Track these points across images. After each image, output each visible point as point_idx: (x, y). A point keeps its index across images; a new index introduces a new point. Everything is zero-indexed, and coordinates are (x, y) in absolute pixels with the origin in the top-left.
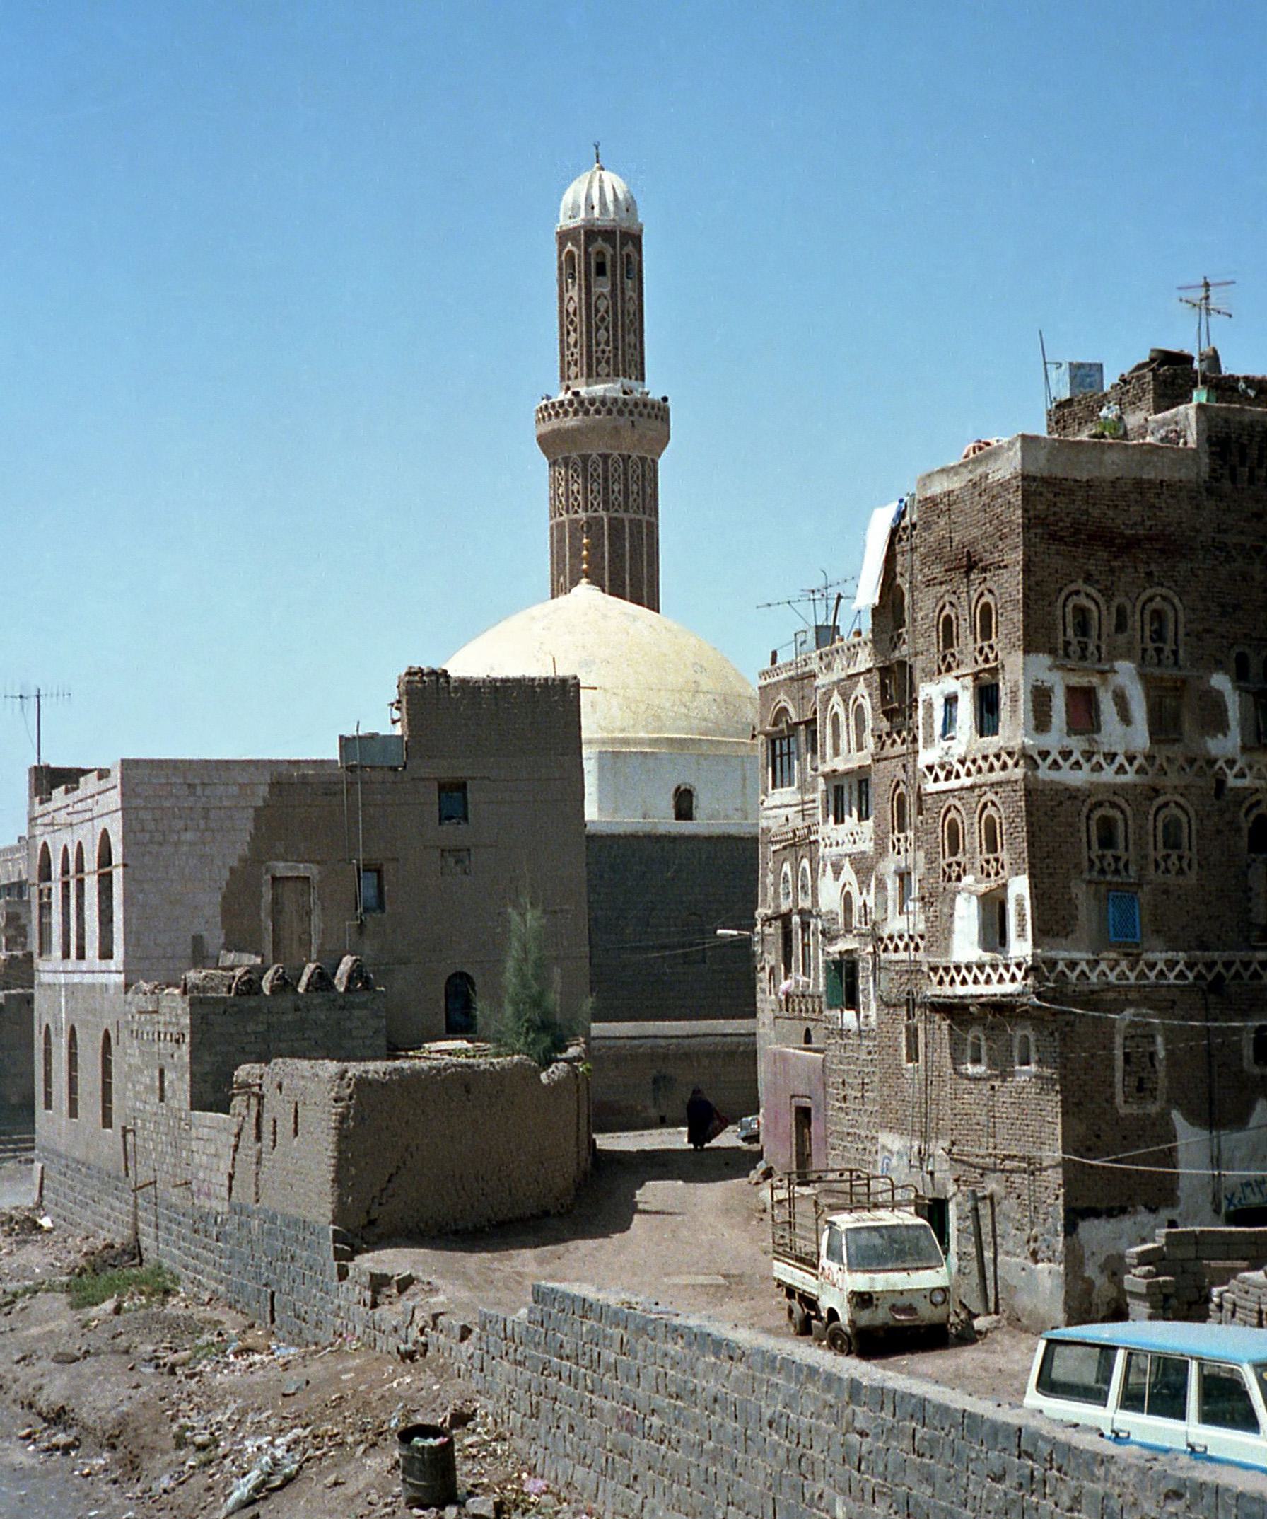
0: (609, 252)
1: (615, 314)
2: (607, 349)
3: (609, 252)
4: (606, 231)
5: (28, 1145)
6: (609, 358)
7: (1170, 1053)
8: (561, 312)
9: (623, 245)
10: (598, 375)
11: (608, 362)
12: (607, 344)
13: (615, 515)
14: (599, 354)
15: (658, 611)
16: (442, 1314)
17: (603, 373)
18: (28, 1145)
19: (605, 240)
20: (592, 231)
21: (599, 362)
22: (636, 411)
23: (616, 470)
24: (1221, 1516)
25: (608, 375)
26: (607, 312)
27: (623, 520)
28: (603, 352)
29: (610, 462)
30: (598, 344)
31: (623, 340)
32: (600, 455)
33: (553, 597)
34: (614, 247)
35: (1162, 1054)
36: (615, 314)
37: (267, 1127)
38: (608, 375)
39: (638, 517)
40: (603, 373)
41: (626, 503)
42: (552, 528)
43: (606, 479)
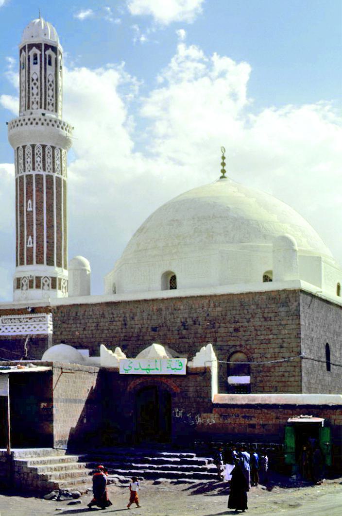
0: (38, 52)
1: (45, 87)
5: (35, 98)
7: (127, 465)
10: (49, 110)
11: (53, 105)
12: (37, 94)
13: (49, 174)
16: (190, 495)
17: (51, 109)
18: (35, 98)
24: (1, 367)
25: (52, 111)
26: (53, 82)
29: (46, 149)
34: (41, 50)
35: (127, 464)
36: (45, 87)
37: (29, 242)
38: (52, 111)
39: (30, 173)
40: (51, 109)
41: (54, 169)
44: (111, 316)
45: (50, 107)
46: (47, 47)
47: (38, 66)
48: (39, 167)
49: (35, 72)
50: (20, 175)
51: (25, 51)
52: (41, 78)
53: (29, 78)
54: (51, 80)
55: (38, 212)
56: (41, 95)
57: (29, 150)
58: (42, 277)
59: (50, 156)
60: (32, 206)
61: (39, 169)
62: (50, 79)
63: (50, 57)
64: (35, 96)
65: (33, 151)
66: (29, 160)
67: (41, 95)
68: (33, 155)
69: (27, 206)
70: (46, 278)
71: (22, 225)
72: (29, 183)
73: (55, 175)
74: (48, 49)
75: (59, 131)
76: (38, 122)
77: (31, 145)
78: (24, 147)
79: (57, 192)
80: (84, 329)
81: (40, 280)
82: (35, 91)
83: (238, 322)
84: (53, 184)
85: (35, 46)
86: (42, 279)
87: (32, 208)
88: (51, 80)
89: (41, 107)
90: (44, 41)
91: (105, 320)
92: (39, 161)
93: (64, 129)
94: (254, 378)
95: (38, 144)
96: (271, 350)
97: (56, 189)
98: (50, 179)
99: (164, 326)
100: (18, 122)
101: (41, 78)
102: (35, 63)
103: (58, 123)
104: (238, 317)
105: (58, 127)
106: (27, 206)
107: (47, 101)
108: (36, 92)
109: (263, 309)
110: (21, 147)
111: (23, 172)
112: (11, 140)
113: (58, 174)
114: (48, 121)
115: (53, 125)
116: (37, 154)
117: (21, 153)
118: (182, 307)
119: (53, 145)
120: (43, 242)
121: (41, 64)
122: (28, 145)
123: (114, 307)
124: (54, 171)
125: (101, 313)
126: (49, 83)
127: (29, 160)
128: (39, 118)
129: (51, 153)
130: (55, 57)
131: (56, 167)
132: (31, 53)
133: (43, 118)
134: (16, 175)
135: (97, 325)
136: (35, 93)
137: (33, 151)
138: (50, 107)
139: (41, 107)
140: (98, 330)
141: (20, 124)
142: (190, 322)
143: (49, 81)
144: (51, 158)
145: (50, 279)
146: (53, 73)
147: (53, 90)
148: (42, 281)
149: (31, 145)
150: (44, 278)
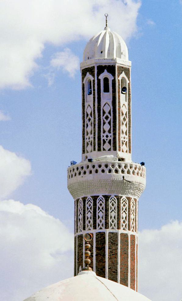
0: (111, 78)
2: (109, 135)
3: (111, 78)
4: (109, 66)
6: (110, 140)
8: (84, 113)
9: (120, 73)
10: (104, 150)
11: (110, 142)
12: (109, 132)
13: (101, 231)
14: (105, 138)
15: (128, 287)
17: (107, 149)
19: (108, 71)
20: (101, 66)
21: (104, 142)
22: (126, 170)
23: (124, 205)
25: (110, 150)
26: (110, 113)
27: (92, 234)
28: (107, 136)
29: (98, 201)
30: (104, 132)
31: (119, 130)
32: (104, 196)
33: (75, 275)
36: (99, 119)
38: (110, 150)
40: (107, 149)
41: (118, 224)
42: (75, 238)
43: (107, 210)
45: (107, 146)
46: (101, 69)
47: (92, 96)
48: (113, 224)
49: (89, 105)
50: (79, 233)
54: (107, 111)
57: (89, 204)
59: (103, 208)
61: (101, 226)
62: (105, 110)
63: (106, 80)
64: (107, 133)
65: (95, 204)
66: (101, 214)
67: (95, 133)
68: (84, 211)
73: (107, 232)
74: (103, 71)
75: (111, 176)
76: (105, 169)
77: (92, 197)
78: (95, 198)
79: (110, 252)
82: (107, 127)
84: (104, 243)
85: (88, 71)
88: (107, 111)
89: (94, 149)
90: (96, 63)
92: (101, 216)
93: (136, 174)
95: (89, 196)
98: (114, 236)
100: (80, 169)
102: (90, 93)
103: (129, 168)
105: (110, 171)
107: (102, 138)
110: (81, 199)
111: (82, 230)
112: (72, 190)
114: (97, 167)
115: (103, 171)
116: (88, 209)
117: (81, 205)
119: (107, 194)
121: (94, 95)
124: (118, 228)
126: (105, 115)
127: (101, 214)
128: (86, 166)
129: (103, 205)
130: (113, 78)
131: (110, 221)
132: (102, 77)
133: (90, 164)
137: (95, 204)
138: (107, 146)
139: (94, 149)
141: (82, 172)
143: (104, 113)
144: (104, 211)
146: (110, 102)
147: (109, 123)
149: (92, 197)
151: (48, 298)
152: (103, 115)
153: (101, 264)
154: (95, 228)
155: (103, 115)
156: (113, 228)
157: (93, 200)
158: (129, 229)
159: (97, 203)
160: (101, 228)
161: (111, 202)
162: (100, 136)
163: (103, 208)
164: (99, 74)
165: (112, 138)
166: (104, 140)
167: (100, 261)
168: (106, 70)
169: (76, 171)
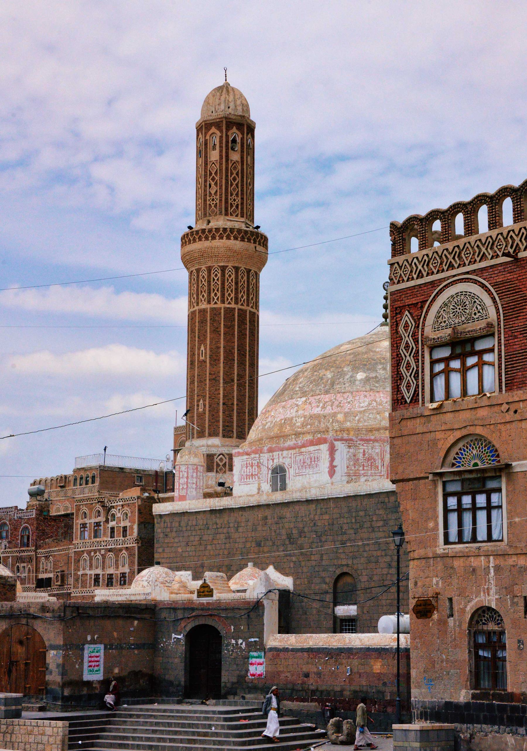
13: (215, 306)
28: (235, 200)
32: (234, 267)
44: (215, 527)
51: (202, 134)
52: (221, 170)
53: (206, 172)
55: (212, 362)
56: (221, 195)
58: (215, 455)
59: (232, 280)
60: (206, 353)
69: (199, 355)
70: (221, 456)
71: (425, 317)
72: (203, 322)
80: (187, 545)
81: (213, 459)
83: (345, 533)
86: (215, 457)
87: (206, 356)
91: (209, 532)
94: (361, 608)
96: (379, 571)
97: (238, 327)
99: (269, 539)
101: (221, 170)
104: (345, 527)
106: (199, 355)
108: (215, 191)
109: (371, 517)
113: (242, 305)
118: (288, 515)
119: (236, 265)
120: (218, 404)
122: (203, 268)
123: (218, 515)
125: (205, 523)
129: (233, 276)
134: (189, 310)
135: (201, 538)
136: (213, 192)
137: (223, 275)
140: (201, 544)
142: (295, 531)
145: (227, 457)
148: (216, 460)
150: (219, 455)
151: (478, 482)
152: (231, 176)
153: (229, 344)
154: (236, 303)
155: (231, 176)
156: (229, 303)
157: (221, 270)
158: (248, 305)
159: (212, 274)
160: (216, 303)
161: (214, 273)
162: (228, 199)
163: (232, 280)
164: (227, 130)
165: (239, 203)
166: (231, 204)
167: (228, 341)
168: (235, 128)
169: (190, 237)
